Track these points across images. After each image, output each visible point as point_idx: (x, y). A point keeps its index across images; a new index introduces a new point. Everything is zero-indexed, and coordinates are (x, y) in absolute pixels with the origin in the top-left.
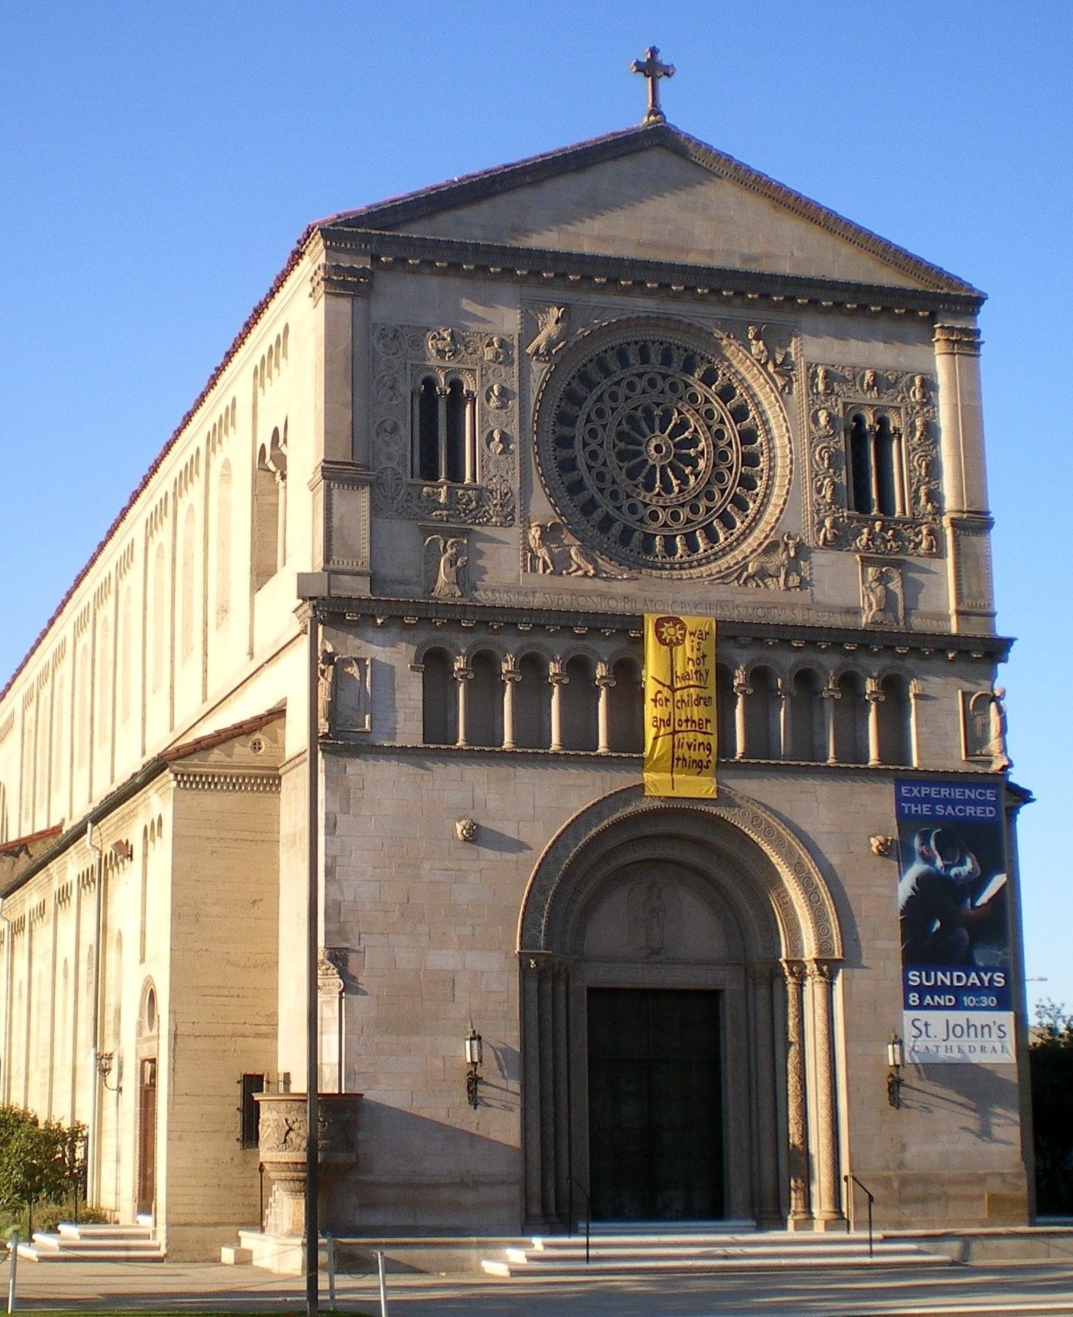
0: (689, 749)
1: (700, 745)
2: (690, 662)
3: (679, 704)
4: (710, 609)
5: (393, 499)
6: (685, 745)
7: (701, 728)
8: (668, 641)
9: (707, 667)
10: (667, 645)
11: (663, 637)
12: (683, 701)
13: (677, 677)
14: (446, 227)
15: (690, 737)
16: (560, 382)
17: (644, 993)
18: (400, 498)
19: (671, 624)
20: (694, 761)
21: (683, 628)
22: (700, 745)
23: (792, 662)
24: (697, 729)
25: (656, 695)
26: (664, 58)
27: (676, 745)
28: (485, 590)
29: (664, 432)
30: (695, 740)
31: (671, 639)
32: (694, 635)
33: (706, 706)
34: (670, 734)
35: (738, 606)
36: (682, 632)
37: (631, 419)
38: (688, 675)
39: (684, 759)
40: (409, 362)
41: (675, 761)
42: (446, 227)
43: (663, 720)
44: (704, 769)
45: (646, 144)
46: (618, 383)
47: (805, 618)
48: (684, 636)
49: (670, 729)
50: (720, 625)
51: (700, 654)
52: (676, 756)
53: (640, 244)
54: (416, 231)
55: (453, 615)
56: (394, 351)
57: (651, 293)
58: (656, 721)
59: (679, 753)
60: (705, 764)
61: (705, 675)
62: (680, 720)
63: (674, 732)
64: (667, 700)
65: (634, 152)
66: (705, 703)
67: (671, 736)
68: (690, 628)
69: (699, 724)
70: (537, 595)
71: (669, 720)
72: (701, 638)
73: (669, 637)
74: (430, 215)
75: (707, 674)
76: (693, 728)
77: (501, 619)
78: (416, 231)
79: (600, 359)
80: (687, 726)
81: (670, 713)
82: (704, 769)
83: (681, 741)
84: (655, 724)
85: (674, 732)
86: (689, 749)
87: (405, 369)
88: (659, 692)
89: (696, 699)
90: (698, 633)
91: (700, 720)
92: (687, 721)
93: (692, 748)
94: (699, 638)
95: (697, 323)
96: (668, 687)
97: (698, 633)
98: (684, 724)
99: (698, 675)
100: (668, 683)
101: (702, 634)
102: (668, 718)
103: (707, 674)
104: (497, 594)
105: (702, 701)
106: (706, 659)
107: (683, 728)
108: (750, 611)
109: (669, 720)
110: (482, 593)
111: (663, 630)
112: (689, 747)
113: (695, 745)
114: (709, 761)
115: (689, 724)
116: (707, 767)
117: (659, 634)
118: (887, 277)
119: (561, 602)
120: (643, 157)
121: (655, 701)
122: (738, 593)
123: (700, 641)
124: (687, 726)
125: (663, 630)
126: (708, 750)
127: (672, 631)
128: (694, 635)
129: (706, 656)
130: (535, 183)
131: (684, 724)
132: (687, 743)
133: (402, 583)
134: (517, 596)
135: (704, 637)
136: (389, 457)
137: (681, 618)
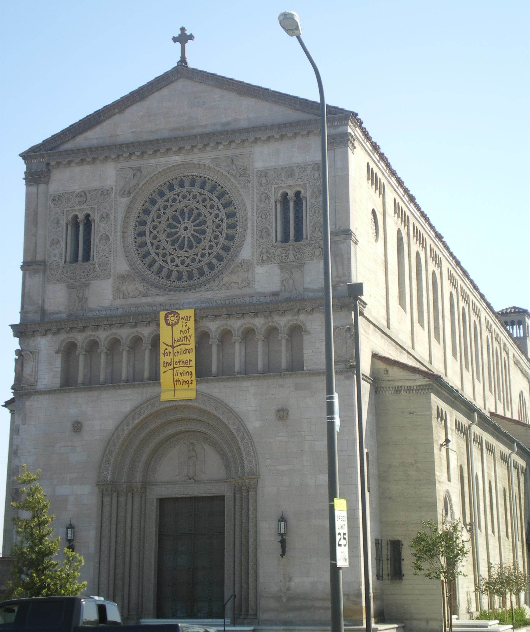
0: (181, 375)
1: (186, 373)
2: (182, 332)
3: (176, 354)
4: (202, 304)
5: (56, 275)
6: (179, 374)
7: (187, 365)
8: (170, 324)
9: (190, 334)
10: (170, 325)
11: (168, 322)
12: (178, 352)
13: (175, 341)
14: (82, 141)
15: (181, 370)
16: (138, 205)
17: (190, 499)
18: (58, 274)
19: (172, 315)
20: (184, 381)
21: (178, 316)
22: (186, 373)
23: (238, 325)
24: (185, 365)
25: (165, 351)
26: (177, 33)
27: (175, 375)
28: (95, 311)
29: (180, 222)
30: (184, 371)
31: (172, 323)
32: (184, 319)
33: (189, 353)
34: (172, 369)
35: (216, 300)
36: (178, 318)
37: (191, 211)
38: (180, 339)
39: (179, 381)
40: (65, 210)
41: (175, 382)
42: (82, 141)
43: (168, 363)
44: (190, 384)
45: (173, 79)
46: (201, 194)
47: (251, 301)
48: (178, 320)
49: (171, 367)
50: (198, 312)
51: (187, 328)
52: (175, 380)
53: (171, 130)
54: (69, 146)
55: (73, 326)
56: (59, 206)
57: (176, 153)
58: (165, 364)
59: (176, 378)
60: (190, 382)
61: (189, 338)
62: (176, 362)
63: (174, 368)
64: (170, 353)
65: (167, 85)
66: (189, 351)
67: (172, 370)
68: (182, 316)
69: (186, 363)
70: (119, 310)
71: (171, 362)
72: (187, 320)
73: (171, 322)
74: (73, 137)
75: (190, 337)
76: (183, 365)
77: (94, 324)
78: (69, 146)
79: (205, 181)
80: (180, 365)
81: (171, 359)
82: (190, 384)
83: (177, 372)
84: (164, 365)
85: (174, 368)
86: (181, 375)
87: (63, 213)
88: (166, 349)
89: (184, 351)
90: (185, 318)
91: (187, 360)
92: (180, 362)
93: (183, 375)
94: (186, 320)
95: (202, 163)
96: (171, 346)
97: (185, 318)
98: (179, 364)
99: (186, 338)
100: (171, 344)
101: (187, 318)
102: (170, 361)
103: (190, 337)
104: (100, 312)
105: (187, 351)
106: (189, 330)
107: (178, 365)
108: (222, 302)
109: (171, 362)
110: (94, 312)
111: (168, 318)
112: (181, 374)
113: (184, 373)
114: (192, 380)
115: (181, 363)
116: (192, 383)
117: (166, 321)
118: (295, 115)
119: (130, 311)
120: (173, 85)
121: (164, 354)
122: (217, 294)
123: (187, 321)
124: (180, 365)
125: (168, 318)
126: (191, 375)
127: (173, 318)
128: (184, 319)
129: (190, 328)
130: (121, 111)
131: (179, 364)
132: (180, 373)
133: (57, 313)
134: (110, 312)
135: (188, 319)
136: (55, 256)
137: (176, 311)
